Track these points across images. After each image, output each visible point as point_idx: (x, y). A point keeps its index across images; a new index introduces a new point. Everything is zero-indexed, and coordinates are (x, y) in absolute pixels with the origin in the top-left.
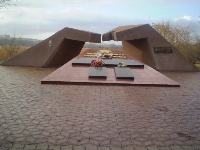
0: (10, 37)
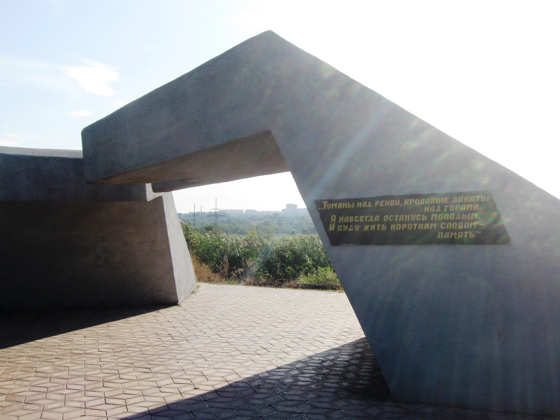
0: (298, 208)
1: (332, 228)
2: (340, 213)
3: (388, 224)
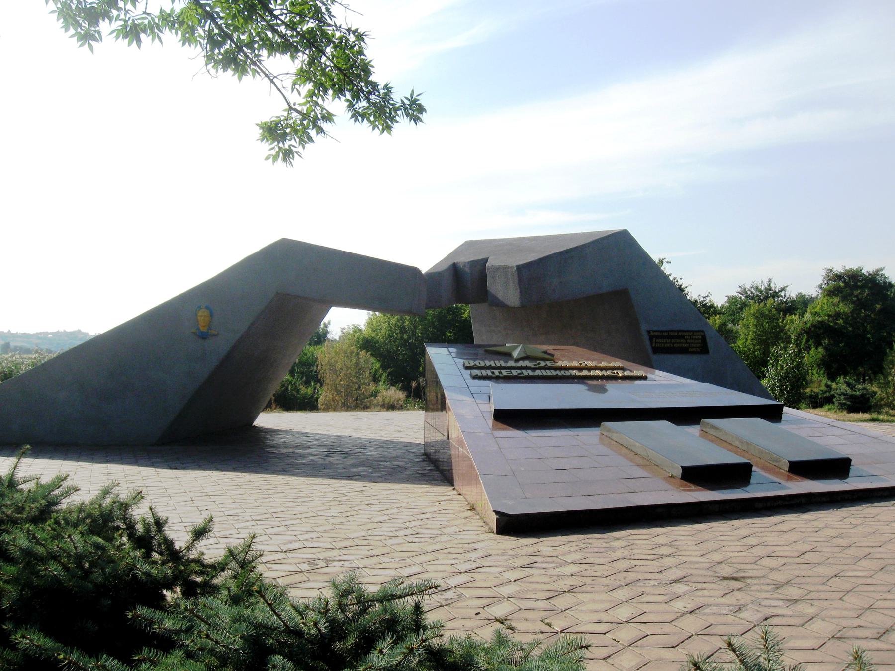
1: (654, 345)
2: (658, 337)
3: (674, 344)
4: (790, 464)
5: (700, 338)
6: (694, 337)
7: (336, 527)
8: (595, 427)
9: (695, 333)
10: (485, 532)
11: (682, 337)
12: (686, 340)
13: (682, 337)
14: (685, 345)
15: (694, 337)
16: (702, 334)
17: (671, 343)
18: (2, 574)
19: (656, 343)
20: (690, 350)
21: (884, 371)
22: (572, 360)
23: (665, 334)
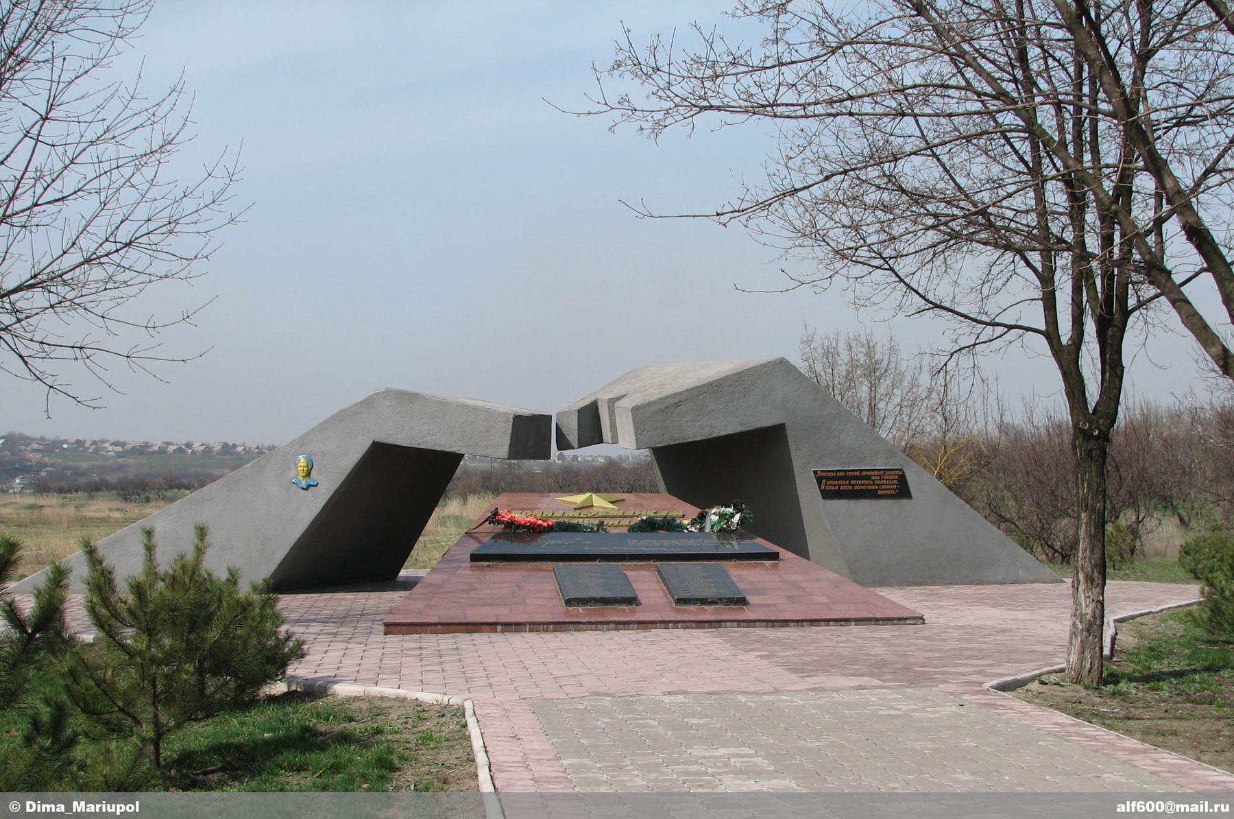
1: (823, 487)
2: (828, 478)
3: (853, 485)
4: (653, 451)
5: (896, 477)
6: (886, 477)
7: (24, 21)
8: (364, 456)
9: (887, 473)
10: (894, 119)
11: (868, 478)
12: (874, 481)
13: (868, 478)
14: (873, 487)
15: (886, 477)
16: (901, 473)
17: (849, 484)
18: (1229, 643)
19: (826, 485)
20: (879, 492)
21: (30, 720)
22: (33, 577)
23: (841, 474)
